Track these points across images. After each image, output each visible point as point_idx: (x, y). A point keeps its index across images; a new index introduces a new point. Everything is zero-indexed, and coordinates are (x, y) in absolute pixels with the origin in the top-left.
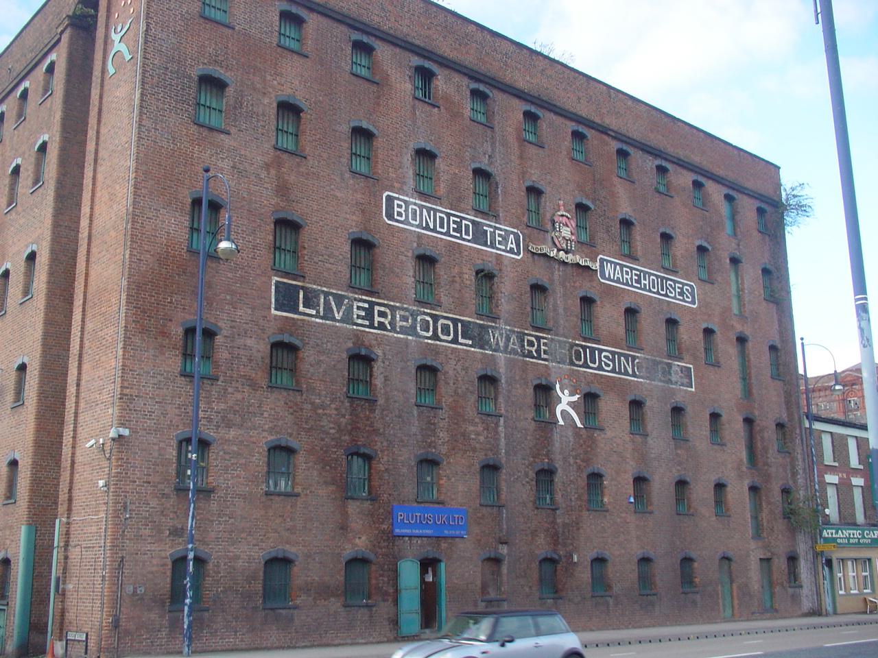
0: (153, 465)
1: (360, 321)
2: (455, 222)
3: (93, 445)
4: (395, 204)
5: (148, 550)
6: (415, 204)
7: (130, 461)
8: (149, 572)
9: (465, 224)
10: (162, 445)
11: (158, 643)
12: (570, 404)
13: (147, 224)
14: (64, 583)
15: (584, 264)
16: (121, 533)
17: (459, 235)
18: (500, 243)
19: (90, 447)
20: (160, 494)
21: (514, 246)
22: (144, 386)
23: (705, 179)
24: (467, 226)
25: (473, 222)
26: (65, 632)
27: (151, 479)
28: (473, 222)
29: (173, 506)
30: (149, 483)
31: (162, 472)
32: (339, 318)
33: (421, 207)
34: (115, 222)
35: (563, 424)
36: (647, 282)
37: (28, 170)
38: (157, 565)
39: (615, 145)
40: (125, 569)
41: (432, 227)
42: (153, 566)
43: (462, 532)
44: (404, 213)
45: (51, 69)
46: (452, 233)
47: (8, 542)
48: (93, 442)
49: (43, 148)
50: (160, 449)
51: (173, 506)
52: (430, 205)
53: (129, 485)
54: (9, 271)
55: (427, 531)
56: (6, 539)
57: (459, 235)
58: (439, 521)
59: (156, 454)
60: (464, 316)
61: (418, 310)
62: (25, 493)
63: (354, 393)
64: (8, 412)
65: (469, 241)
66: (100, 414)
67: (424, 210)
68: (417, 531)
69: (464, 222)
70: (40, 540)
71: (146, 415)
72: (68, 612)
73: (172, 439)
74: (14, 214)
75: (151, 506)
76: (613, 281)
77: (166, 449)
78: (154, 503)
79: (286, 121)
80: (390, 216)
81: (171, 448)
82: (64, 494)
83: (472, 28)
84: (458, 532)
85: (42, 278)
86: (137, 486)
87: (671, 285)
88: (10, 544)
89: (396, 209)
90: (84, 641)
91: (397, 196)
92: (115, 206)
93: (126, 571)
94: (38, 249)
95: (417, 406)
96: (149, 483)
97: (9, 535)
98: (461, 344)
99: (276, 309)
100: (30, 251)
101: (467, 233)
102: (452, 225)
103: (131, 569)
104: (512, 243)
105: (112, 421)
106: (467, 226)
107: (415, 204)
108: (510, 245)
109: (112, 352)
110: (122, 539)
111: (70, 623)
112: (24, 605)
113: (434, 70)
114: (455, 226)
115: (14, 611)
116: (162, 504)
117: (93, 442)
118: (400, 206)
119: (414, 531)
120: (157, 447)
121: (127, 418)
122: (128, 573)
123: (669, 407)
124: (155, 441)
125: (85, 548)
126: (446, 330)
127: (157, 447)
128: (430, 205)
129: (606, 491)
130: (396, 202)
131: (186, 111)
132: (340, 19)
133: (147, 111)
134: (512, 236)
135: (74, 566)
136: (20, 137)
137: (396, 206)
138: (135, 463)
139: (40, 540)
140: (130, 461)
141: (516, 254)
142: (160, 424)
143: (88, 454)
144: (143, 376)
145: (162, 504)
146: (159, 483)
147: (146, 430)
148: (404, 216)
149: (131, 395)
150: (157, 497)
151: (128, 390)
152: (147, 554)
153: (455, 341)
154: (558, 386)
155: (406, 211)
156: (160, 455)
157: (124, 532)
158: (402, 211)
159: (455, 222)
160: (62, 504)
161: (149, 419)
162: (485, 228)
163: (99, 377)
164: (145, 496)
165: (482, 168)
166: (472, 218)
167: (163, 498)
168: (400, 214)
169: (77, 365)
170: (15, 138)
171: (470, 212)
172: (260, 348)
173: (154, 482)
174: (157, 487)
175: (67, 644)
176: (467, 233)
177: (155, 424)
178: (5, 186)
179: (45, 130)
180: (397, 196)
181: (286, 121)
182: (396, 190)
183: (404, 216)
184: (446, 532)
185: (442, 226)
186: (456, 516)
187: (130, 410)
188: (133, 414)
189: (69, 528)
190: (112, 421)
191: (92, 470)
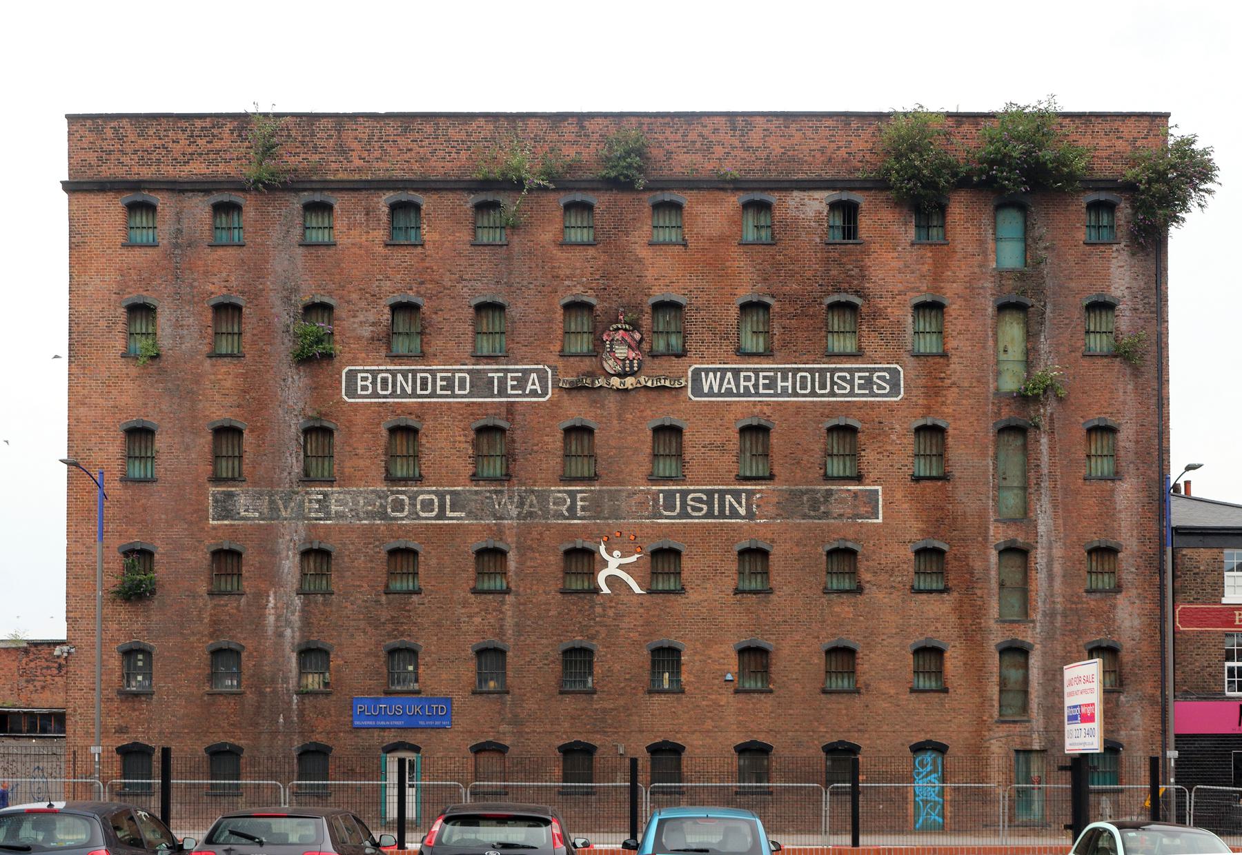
1: (313, 515)
12: (621, 567)
15: (655, 385)
18: (513, 387)
21: (537, 387)
23: (241, 194)
28: (469, 372)
29: (118, 708)
31: (106, 680)
32: (727, 496)
35: (610, 592)
36: (789, 384)
39: (384, 200)
44: (370, 386)
51: (118, 708)
55: (368, 723)
60: (455, 486)
76: (720, 395)
83: (1129, 129)
87: (843, 378)
89: (360, 383)
91: (361, 368)
99: (877, 491)
101: (462, 387)
104: (534, 384)
108: (529, 387)
113: (767, 199)
123: (822, 550)
129: (683, 668)
132: (352, 187)
134: (534, 376)
141: (540, 396)
154: (602, 548)
157: (75, 731)
161: (92, 636)
162: (490, 375)
171: (467, 362)
172: (201, 558)
182: (360, 361)
185: (803, 378)
187: (75, 630)
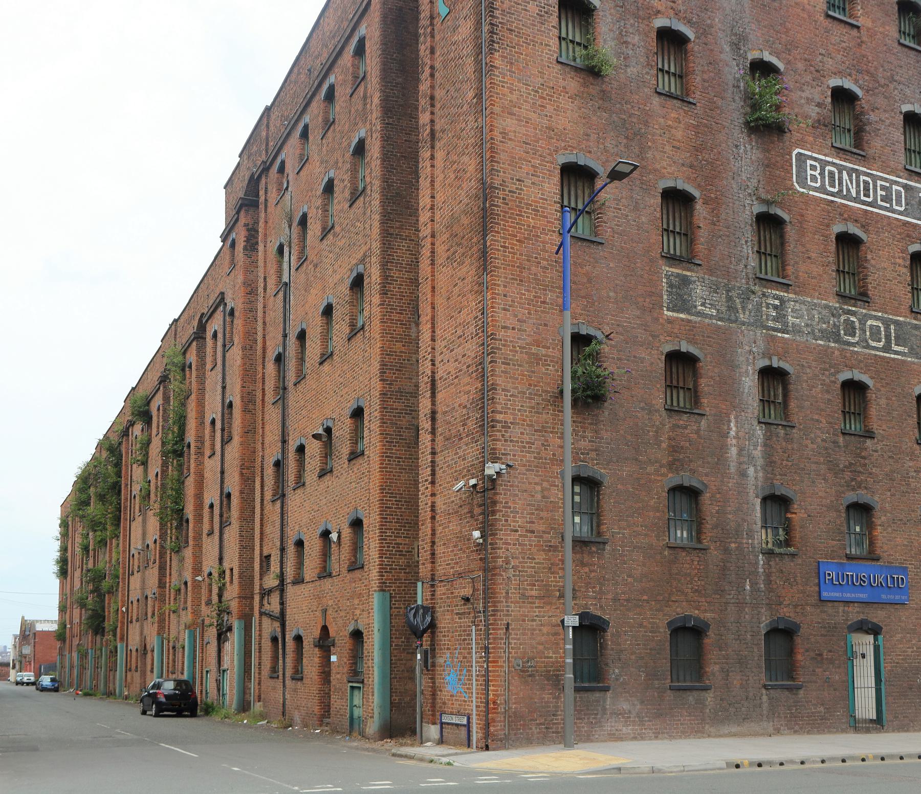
0: (537, 510)
1: (771, 324)
2: (883, 188)
3: (462, 488)
4: (808, 165)
5: (537, 616)
6: (833, 164)
7: (509, 504)
8: (539, 644)
9: (896, 190)
10: (545, 484)
11: (554, 730)
13: (510, 200)
14: (434, 657)
16: (504, 595)
17: (888, 205)
19: (457, 491)
20: (546, 546)
22: (519, 410)
24: (898, 194)
25: (905, 187)
26: (438, 714)
27: (535, 527)
28: (905, 187)
30: (533, 532)
33: (841, 169)
34: (467, 205)
37: (343, 181)
38: (548, 634)
40: (512, 639)
41: (854, 195)
42: (543, 635)
43: (903, 597)
44: (819, 177)
45: (360, 51)
46: (879, 202)
47: (358, 612)
48: (461, 483)
49: (360, 149)
50: (543, 490)
52: (851, 166)
53: (510, 535)
54: (332, 305)
56: (356, 609)
57: (888, 205)
58: (875, 583)
59: (539, 496)
61: (841, 309)
62: (375, 555)
63: (764, 417)
64: (346, 466)
65: (900, 213)
66: (465, 450)
67: (845, 173)
68: (849, 595)
69: (895, 187)
70: (395, 608)
71: (525, 447)
72: (441, 691)
73: (557, 477)
74: (331, 238)
75: (537, 561)
77: (550, 489)
78: (541, 557)
79: (666, 57)
80: (803, 183)
81: (556, 488)
82: (425, 552)
84: (897, 597)
85: (374, 300)
86: (520, 536)
88: (360, 615)
89: (809, 172)
90: (464, 725)
91: (809, 153)
92: (465, 185)
93: (513, 642)
94: (365, 270)
95: (844, 434)
96: (533, 532)
97: (358, 604)
98: (896, 353)
100: (355, 275)
101: (899, 203)
102: (880, 192)
103: (519, 639)
105: (483, 457)
106: (898, 194)
107: (833, 164)
109: (478, 370)
110: (506, 602)
111: (444, 703)
112: (383, 677)
114: (884, 193)
115: (373, 688)
116: (549, 560)
117: (461, 483)
118: (813, 168)
119: (845, 595)
120: (538, 488)
121: (503, 452)
122: (515, 643)
124: (537, 480)
125: (457, 614)
126: (875, 333)
127: (538, 488)
128: (851, 166)
130: (809, 162)
131: (546, 45)
133: (499, 47)
135: (444, 636)
136: (330, 145)
137: (808, 168)
138: (515, 508)
139: (395, 608)
140: (509, 504)
142: (541, 458)
143: (453, 501)
144: (518, 397)
145: (549, 560)
146: (544, 532)
147: (525, 465)
148: (819, 180)
149: (505, 422)
150: (544, 550)
151: (502, 416)
152: (535, 620)
153: (887, 348)
155: (822, 174)
156: (543, 497)
157: (507, 593)
158: (817, 173)
159: (883, 188)
160: (423, 564)
163: (460, 405)
164: (530, 549)
165: (916, 111)
166: (905, 181)
167: (550, 551)
168: (814, 179)
169: (429, 395)
170: (324, 149)
173: (538, 532)
174: (541, 537)
175: (442, 728)
176: (899, 203)
177: (535, 458)
178: (318, 208)
179: (360, 124)
180: (809, 153)
181: (666, 57)
183: (819, 180)
184: (884, 596)
186: (895, 576)
187: (506, 441)
188: (509, 446)
189: (434, 591)
190: (483, 457)
191: (460, 520)
